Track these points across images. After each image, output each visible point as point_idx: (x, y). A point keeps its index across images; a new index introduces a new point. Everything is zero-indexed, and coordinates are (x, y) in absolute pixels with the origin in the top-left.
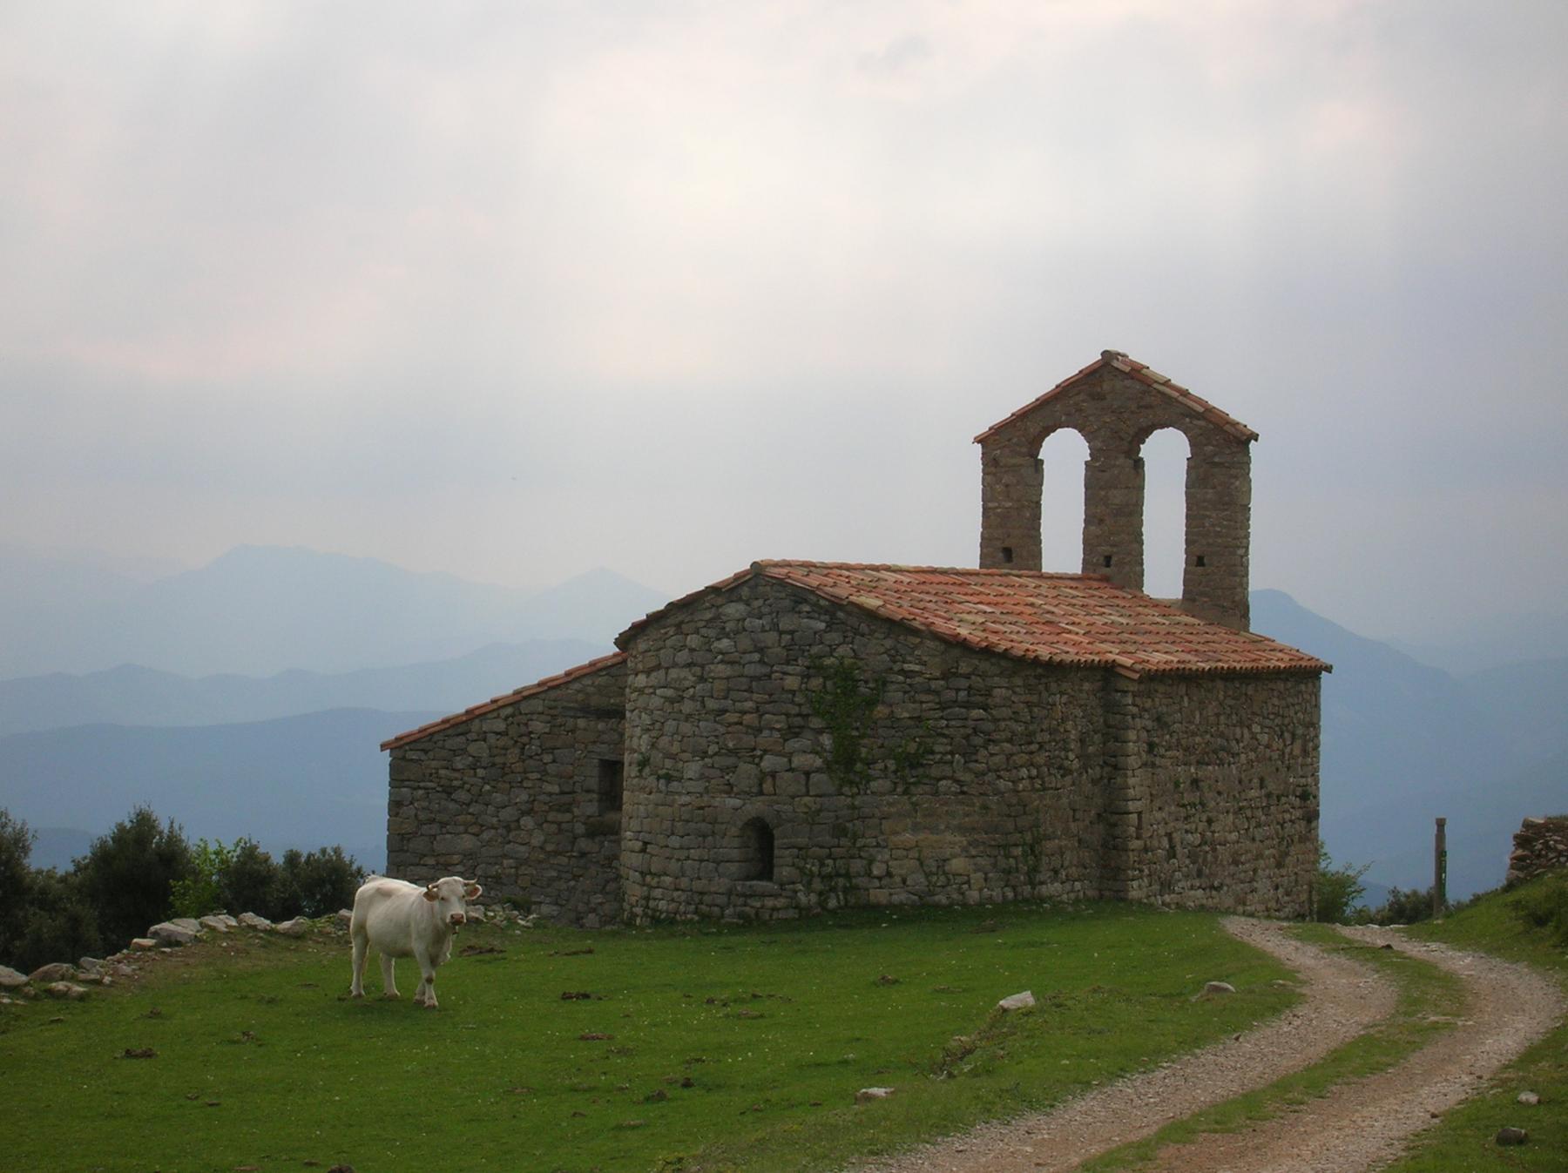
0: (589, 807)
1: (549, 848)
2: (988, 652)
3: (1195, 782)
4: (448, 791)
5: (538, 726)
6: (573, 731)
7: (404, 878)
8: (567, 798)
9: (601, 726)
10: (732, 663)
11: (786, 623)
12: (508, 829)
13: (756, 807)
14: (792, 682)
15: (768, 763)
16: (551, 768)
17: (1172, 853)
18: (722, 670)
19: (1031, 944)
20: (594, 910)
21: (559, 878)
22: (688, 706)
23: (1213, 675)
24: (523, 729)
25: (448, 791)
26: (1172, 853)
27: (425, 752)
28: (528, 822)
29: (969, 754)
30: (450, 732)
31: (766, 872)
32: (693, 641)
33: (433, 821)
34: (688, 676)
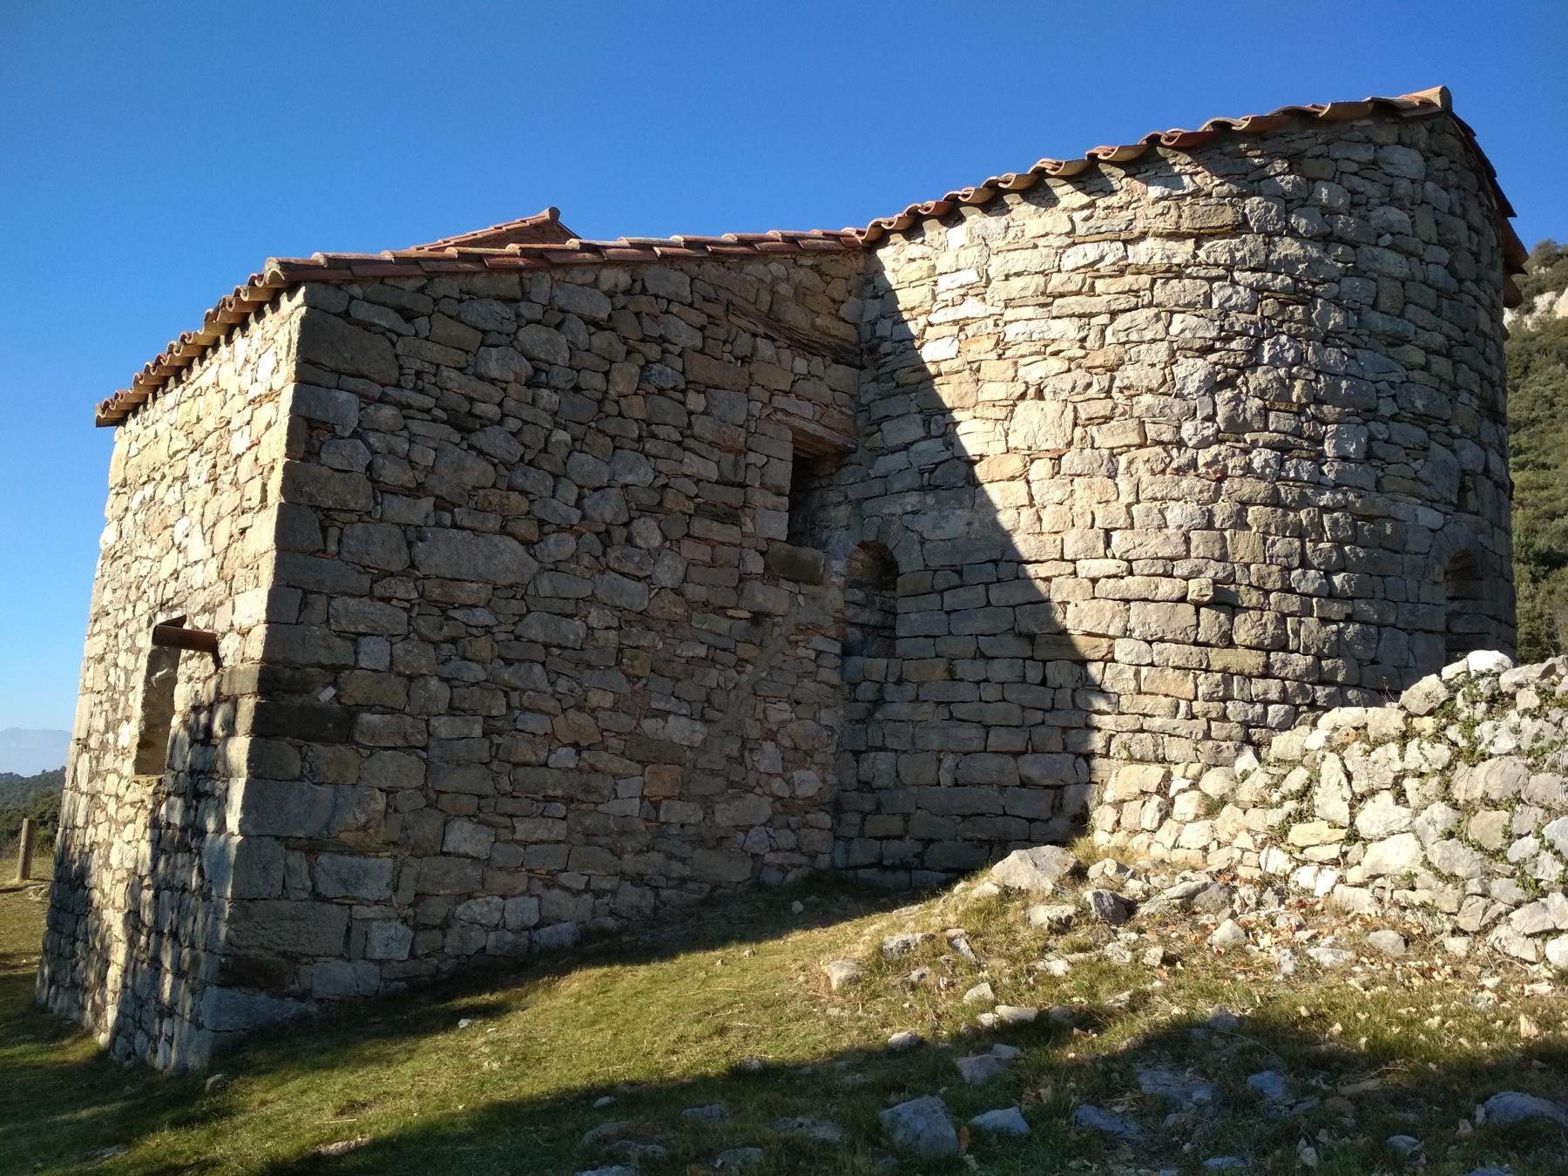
1: (695, 592)
4: (464, 423)
6: (744, 360)
8: (732, 496)
9: (800, 365)
10: (1409, 255)
12: (605, 538)
16: (701, 426)
18: (1393, 263)
20: (771, 736)
21: (710, 661)
24: (655, 331)
27: (408, 315)
28: (648, 533)
30: (479, 282)
33: (415, 492)
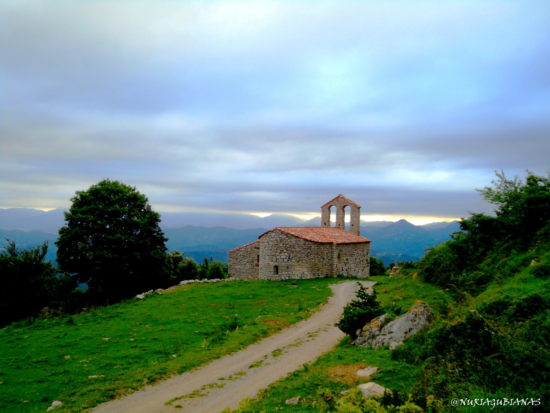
0: (256, 262)
2: (310, 241)
3: (347, 260)
4: (237, 259)
5: (249, 250)
7: (419, 227)
11: (280, 236)
13: (276, 264)
14: (281, 245)
15: (278, 257)
17: (343, 270)
19: (136, 305)
22: (267, 248)
23: (350, 243)
25: (237, 259)
26: (343, 270)
29: (308, 256)
31: (277, 274)
32: (268, 239)
34: (267, 244)
